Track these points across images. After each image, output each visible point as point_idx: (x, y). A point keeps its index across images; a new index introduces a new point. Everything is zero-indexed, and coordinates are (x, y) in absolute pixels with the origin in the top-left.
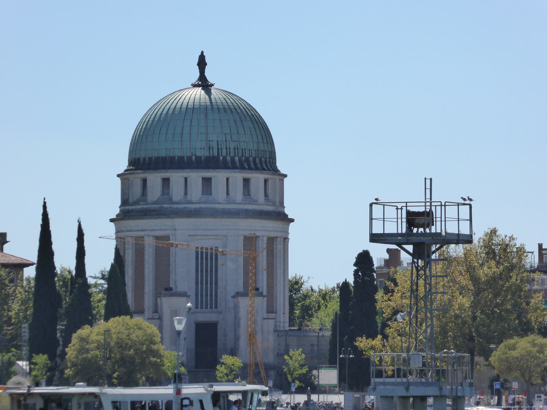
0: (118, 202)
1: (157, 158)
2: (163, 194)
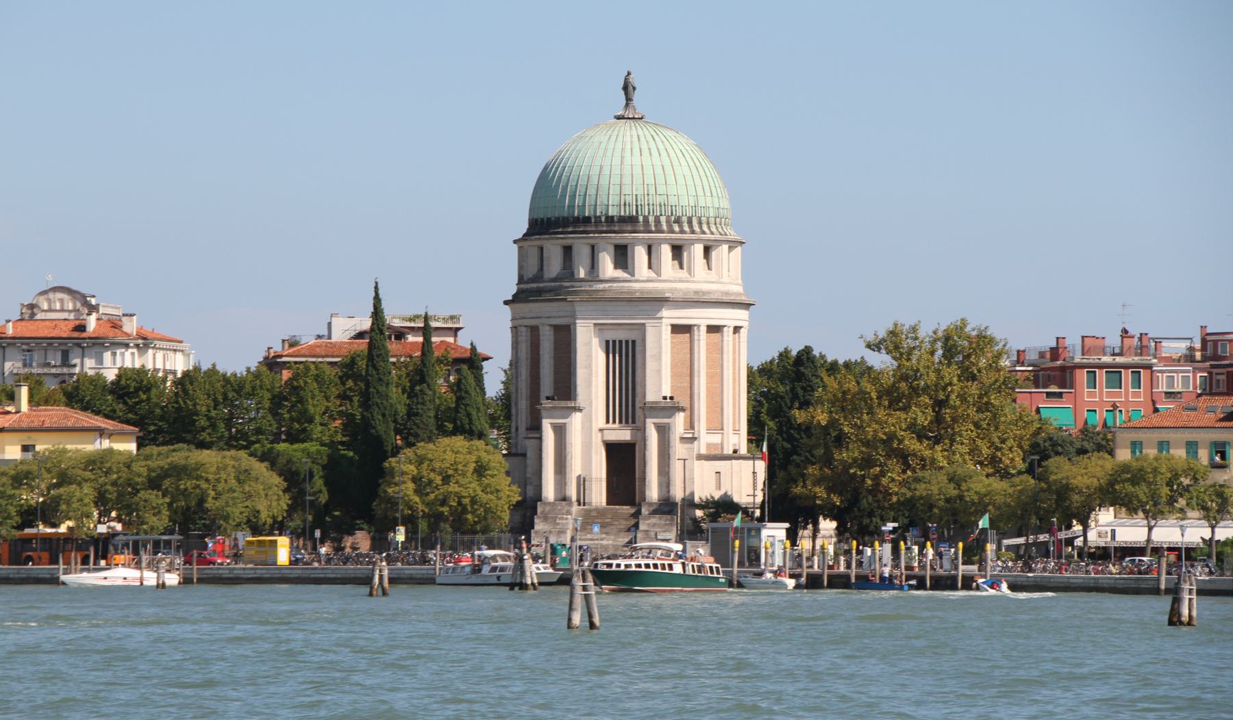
2: (564, 269)
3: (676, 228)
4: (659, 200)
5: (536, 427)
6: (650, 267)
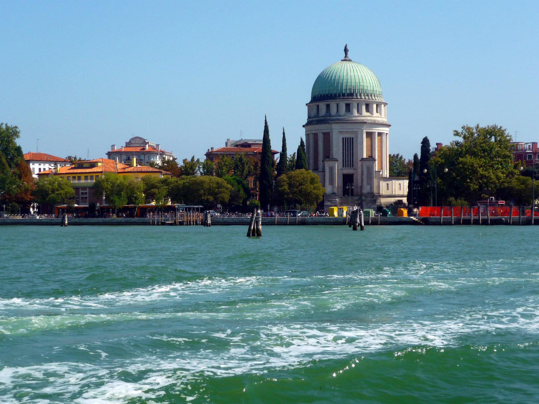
1: (324, 95)
3: (367, 98)
6: (377, 112)
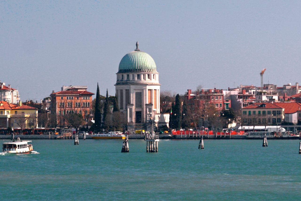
0: (116, 80)
2: (127, 79)
4: (145, 66)
5: (126, 109)
